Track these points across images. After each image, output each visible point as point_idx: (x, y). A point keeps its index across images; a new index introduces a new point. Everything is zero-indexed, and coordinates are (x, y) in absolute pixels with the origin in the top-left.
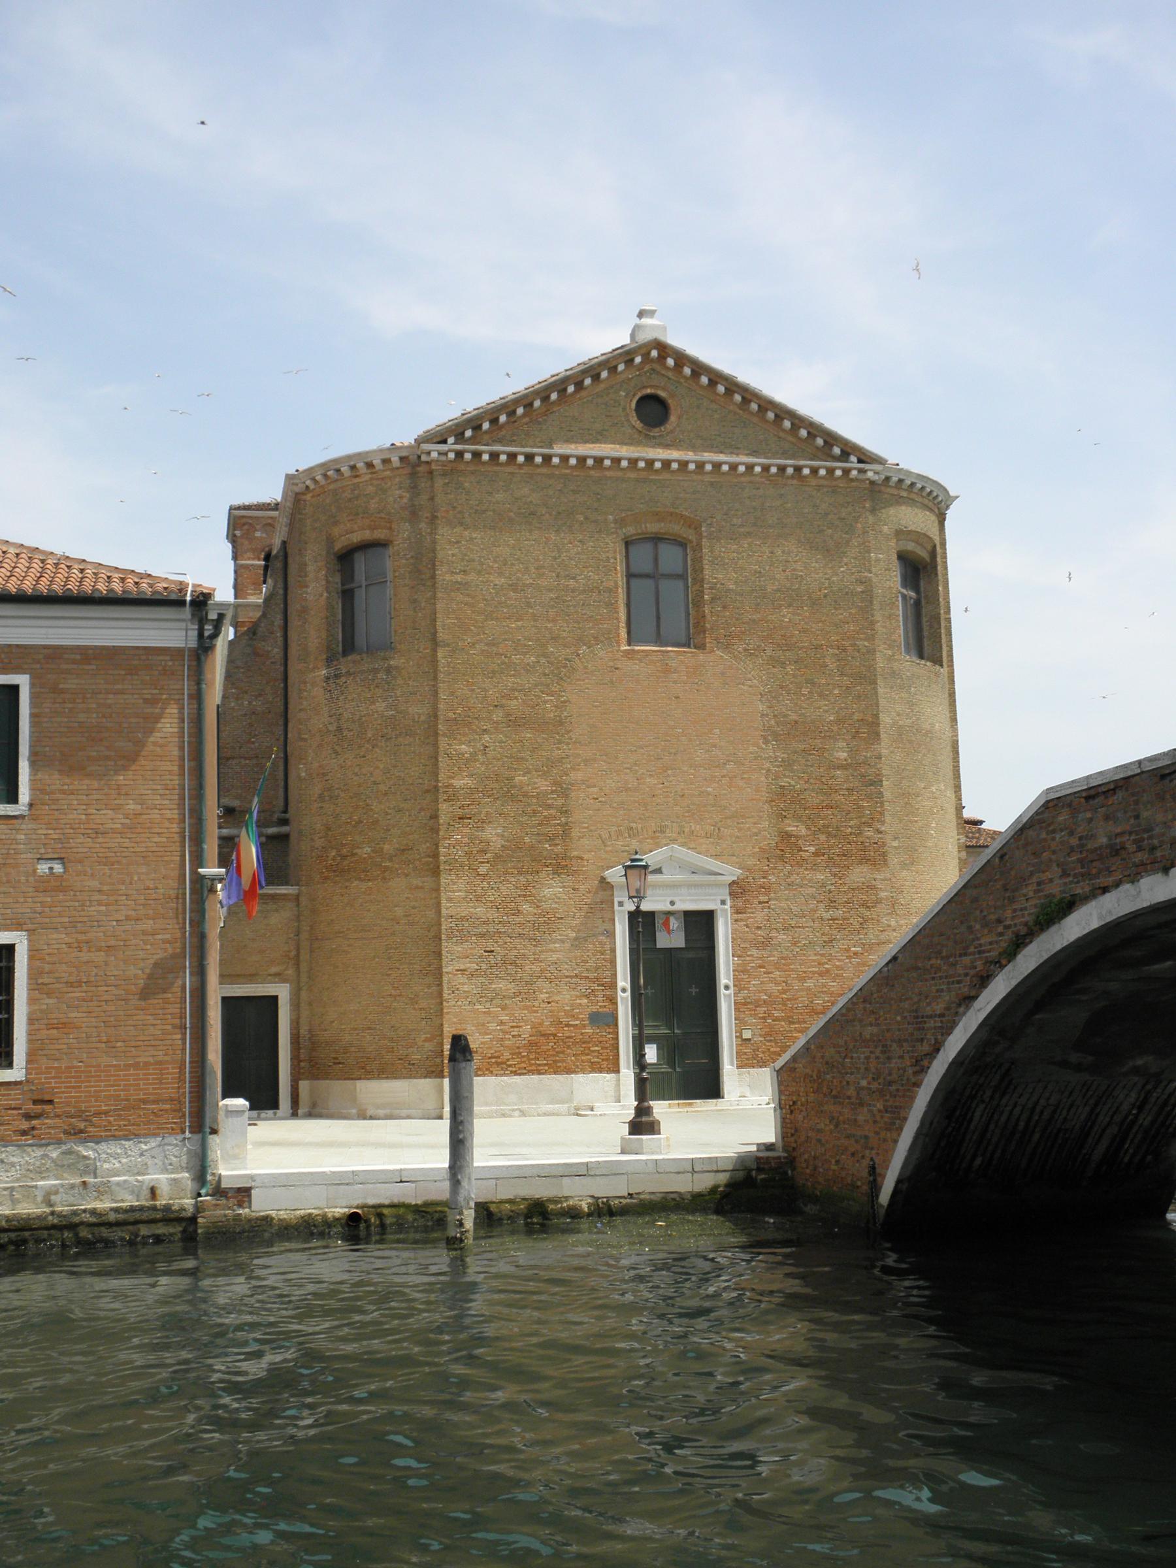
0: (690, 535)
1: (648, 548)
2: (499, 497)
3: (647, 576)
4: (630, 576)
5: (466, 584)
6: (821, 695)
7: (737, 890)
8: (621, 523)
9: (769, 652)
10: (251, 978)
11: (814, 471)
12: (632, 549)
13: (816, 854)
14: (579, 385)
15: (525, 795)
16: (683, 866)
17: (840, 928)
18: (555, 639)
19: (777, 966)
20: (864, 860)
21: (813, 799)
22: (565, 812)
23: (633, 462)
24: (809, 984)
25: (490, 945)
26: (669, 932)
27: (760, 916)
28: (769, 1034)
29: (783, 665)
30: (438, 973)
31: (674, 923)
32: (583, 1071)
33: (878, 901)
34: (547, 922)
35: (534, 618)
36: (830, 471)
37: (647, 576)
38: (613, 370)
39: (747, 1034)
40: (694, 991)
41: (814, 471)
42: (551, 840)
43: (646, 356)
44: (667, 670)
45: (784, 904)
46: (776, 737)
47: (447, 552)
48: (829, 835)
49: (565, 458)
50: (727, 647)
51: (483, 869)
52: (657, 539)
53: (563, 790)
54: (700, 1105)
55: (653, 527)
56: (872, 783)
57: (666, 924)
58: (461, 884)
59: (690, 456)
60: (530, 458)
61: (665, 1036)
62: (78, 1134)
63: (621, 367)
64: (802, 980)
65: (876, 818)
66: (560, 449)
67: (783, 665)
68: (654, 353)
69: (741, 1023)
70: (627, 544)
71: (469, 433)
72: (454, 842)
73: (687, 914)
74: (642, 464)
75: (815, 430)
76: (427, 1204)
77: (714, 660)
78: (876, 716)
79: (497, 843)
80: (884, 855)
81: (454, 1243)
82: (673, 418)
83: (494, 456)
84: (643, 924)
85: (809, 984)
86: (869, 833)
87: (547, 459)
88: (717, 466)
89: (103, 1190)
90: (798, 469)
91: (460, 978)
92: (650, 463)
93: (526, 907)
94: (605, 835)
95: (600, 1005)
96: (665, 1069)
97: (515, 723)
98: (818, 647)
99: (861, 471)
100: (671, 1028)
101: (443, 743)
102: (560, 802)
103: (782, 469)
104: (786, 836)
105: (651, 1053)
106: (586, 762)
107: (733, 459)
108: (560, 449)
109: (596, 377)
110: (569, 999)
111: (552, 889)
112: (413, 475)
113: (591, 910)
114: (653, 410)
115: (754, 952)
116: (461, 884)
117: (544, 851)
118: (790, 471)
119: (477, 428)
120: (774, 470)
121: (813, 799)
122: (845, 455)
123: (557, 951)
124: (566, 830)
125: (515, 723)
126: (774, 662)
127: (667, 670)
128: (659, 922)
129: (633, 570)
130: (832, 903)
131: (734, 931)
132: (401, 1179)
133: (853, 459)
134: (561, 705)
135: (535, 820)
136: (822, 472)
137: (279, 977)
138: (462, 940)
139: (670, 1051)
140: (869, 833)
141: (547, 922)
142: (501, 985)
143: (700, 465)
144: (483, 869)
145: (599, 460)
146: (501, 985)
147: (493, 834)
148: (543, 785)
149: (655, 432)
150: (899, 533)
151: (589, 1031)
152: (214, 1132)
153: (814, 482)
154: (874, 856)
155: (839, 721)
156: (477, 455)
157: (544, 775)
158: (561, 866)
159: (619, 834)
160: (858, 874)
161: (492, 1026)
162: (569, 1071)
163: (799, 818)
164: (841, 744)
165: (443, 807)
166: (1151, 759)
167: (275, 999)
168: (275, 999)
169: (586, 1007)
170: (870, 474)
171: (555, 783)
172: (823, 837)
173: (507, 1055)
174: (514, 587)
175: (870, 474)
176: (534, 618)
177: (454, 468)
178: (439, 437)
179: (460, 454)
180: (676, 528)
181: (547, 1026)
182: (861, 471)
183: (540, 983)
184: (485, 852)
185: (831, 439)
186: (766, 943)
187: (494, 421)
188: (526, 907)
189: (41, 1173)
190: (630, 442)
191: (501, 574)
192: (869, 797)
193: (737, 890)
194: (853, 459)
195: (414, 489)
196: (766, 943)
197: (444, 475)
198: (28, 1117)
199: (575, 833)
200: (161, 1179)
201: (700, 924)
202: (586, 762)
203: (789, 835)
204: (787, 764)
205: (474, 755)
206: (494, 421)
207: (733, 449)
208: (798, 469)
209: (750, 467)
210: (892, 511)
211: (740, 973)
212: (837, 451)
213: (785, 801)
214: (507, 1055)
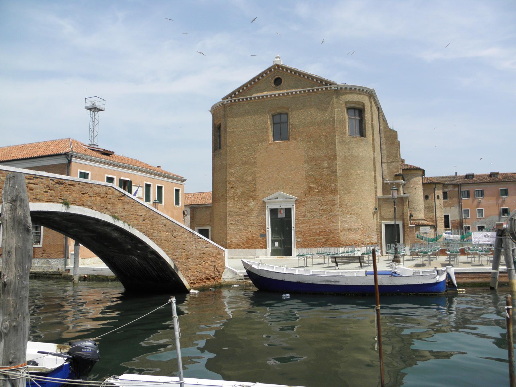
0: (286, 111)
1: (278, 117)
2: (241, 109)
3: (278, 123)
4: (274, 124)
5: (233, 132)
6: (320, 149)
7: (297, 202)
8: (270, 111)
9: (306, 139)
10: (203, 225)
11: (317, 90)
12: (275, 117)
13: (318, 192)
14: (258, 79)
15: (246, 181)
16: (284, 197)
17: (324, 212)
18: (253, 142)
19: (307, 222)
20: (332, 193)
21: (318, 177)
22: (255, 184)
23: (271, 95)
24: (316, 227)
25: (238, 217)
26: (281, 213)
27: (303, 209)
28: (305, 240)
29: (310, 142)
30: (226, 224)
31: (282, 211)
32: (258, 248)
33: (335, 204)
34: (250, 212)
35: (249, 138)
36: (322, 89)
37: (278, 123)
38: (266, 73)
39: (299, 240)
40: (287, 228)
41: (317, 90)
42: (252, 192)
43: (275, 69)
44: (280, 147)
45: (309, 206)
46: (308, 161)
47: (229, 125)
48: (322, 187)
49: (254, 98)
50: (296, 139)
51: (236, 200)
52: (280, 114)
53: (255, 180)
54: (285, 258)
55: (278, 111)
56: (334, 172)
57: (280, 211)
58: (232, 203)
59: (285, 91)
60: (247, 99)
61: (280, 240)
62: (49, 257)
63: (268, 72)
64: (314, 225)
65: (335, 181)
66: (253, 96)
67: (310, 142)
68: (276, 67)
69: (297, 237)
70: (273, 116)
71: (233, 96)
72: (230, 193)
73: (286, 209)
74: (273, 96)
75: (318, 79)
76: (98, 275)
77: (292, 143)
78: (336, 153)
79: (240, 193)
80: (337, 191)
81: (74, 284)
82: (282, 83)
83: (239, 100)
84: (274, 212)
85: (316, 227)
86: (333, 185)
87: (251, 98)
88: (292, 93)
89: (52, 268)
90: (313, 90)
91: (231, 226)
92: (275, 95)
93: (246, 208)
94: (264, 190)
95: (262, 232)
96: (280, 248)
97: (244, 164)
98: (320, 136)
99: (330, 88)
100: (281, 237)
101: (228, 170)
102: (254, 182)
103: (309, 91)
104: (310, 188)
105: (276, 244)
106: (260, 172)
107: (296, 90)
108: (253, 96)
109: (262, 76)
110: (256, 230)
111: (252, 204)
112: (224, 107)
113: (261, 209)
114: (278, 82)
115: (301, 218)
116: (232, 203)
117: (250, 195)
118: (311, 91)
119: (235, 94)
120: (307, 91)
121: (318, 177)
122: (326, 84)
123: (253, 219)
124: (255, 189)
125: (244, 164)
126: (307, 142)
127: (280, 147)
128: (279, 211)
129: (275, 122)
130: (322, 205)
131: (296, 213)
132: (94, 270)
133: (328, 85)
134: (255, 158)
135: (248, 187)
136: (320, 90)
137: (209, 225)
138: (232, 216)
139: (281, 243)
140: (333, 185)
141: (250, 212)
142: (240, 227)
143: (288, 93)
144: (236, 200)
145: (263, 97)
146: (240, 227)
147: (239, 191)
148: (250, 178)
149: (278, 87)
150: (346, 103)
151: (260, 238)
152: (68, 258)
153: (319, 93)
154: (334, 192)
155: (325, 156)
156: (235, 100)
157: (251, 176)
158: (254, 198)
159: (268, 189)
160: (330, 197)
161: (238, 237)
162: (255, 248)
163: (314, 183)
164: (326, 162)
165: (228, 185)
166: (127, 159)
167: (208, 230)
168: (208, 230)
169: (259, 232)
170: (333, 88)
171: (253, 178)
172: (320, 187)
173: (241, 244)
174: (244, 131)
175: (333, 88)
176: (249, 138)
177: (231, 105)
178: (226, 98)
179: (231, 101)
180: (284, 110)
181: (250, 237)
182: (330, 88)
183: (249, 227)
184: (237, 195)
185: (322, 80)
186: (304, 216)
187: (239, 92)
188: (246, 208)
189: (44, 264)
190: (272, 90)
191: (241, 128)
192: (333, 176)
193: (297, 202)
194: (328, 85)
195: (225, 111)
196: (304, 216)
197: (229, 106)
198: (43, 254)
199: (257, 190)
200: (60, 266)
201: (288, 211)
202: (260, 172)
203: (311, 187)
204: (311, 169)
205: (235, 172)
206: (239, 92)
207: (297, 87)
208: (313, 90)
209: (300, 92)
210: (343, 97)
211: (297, 224)
212: (324, 83)
213: (310, 178)
214: (241, 244)
